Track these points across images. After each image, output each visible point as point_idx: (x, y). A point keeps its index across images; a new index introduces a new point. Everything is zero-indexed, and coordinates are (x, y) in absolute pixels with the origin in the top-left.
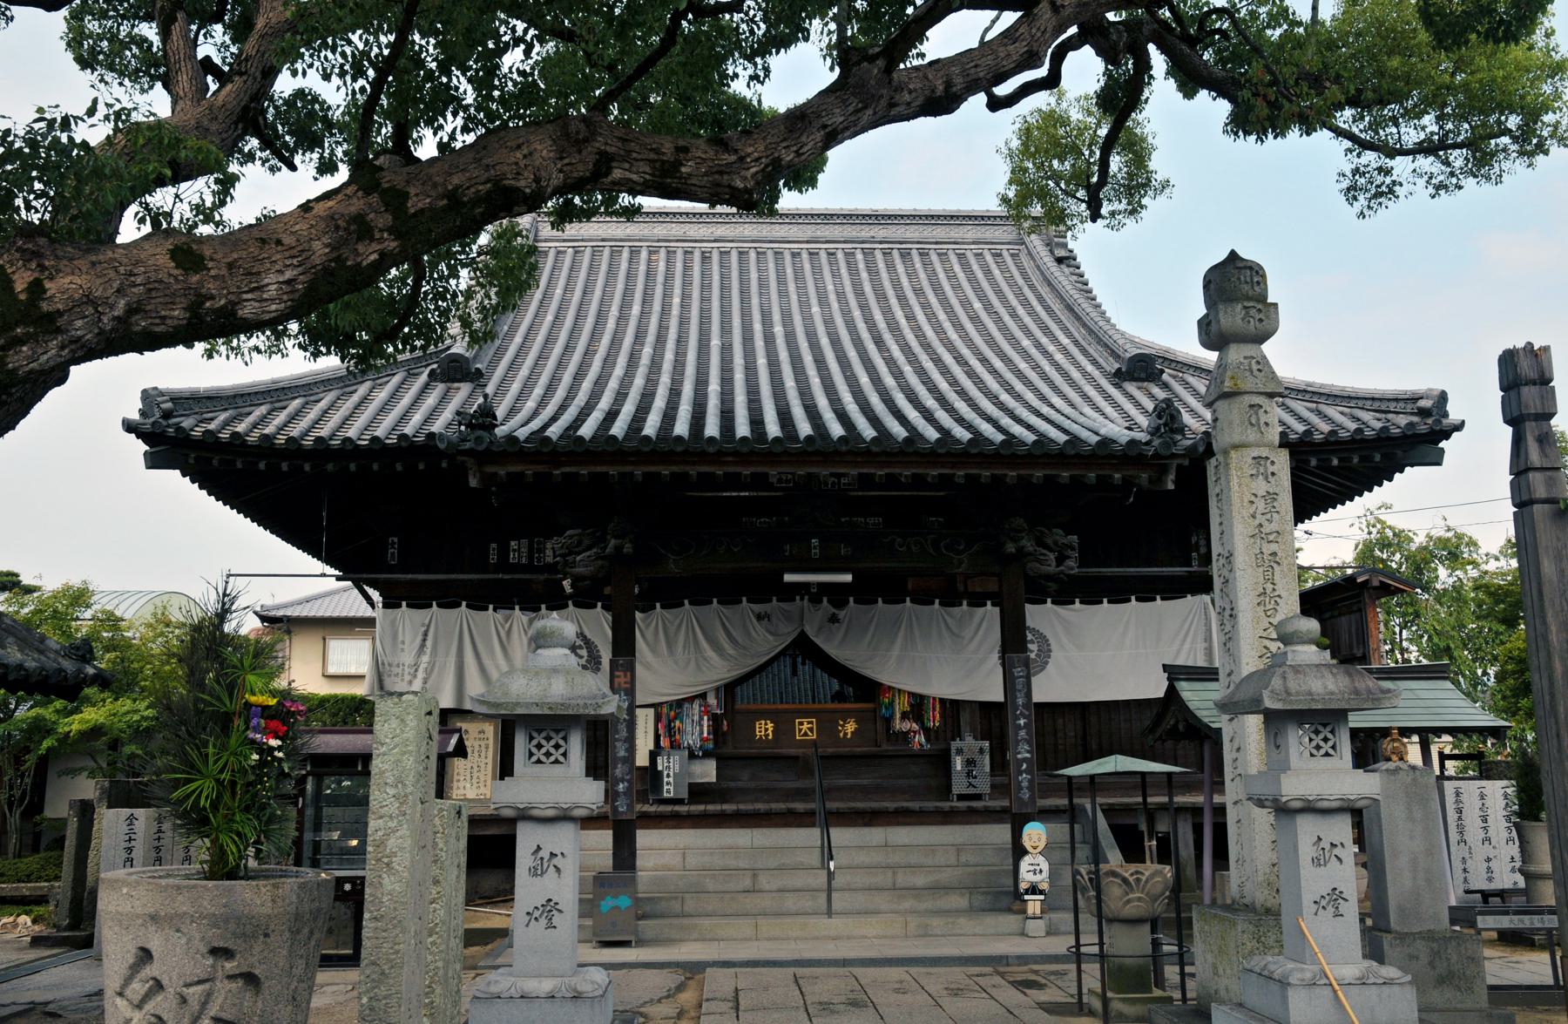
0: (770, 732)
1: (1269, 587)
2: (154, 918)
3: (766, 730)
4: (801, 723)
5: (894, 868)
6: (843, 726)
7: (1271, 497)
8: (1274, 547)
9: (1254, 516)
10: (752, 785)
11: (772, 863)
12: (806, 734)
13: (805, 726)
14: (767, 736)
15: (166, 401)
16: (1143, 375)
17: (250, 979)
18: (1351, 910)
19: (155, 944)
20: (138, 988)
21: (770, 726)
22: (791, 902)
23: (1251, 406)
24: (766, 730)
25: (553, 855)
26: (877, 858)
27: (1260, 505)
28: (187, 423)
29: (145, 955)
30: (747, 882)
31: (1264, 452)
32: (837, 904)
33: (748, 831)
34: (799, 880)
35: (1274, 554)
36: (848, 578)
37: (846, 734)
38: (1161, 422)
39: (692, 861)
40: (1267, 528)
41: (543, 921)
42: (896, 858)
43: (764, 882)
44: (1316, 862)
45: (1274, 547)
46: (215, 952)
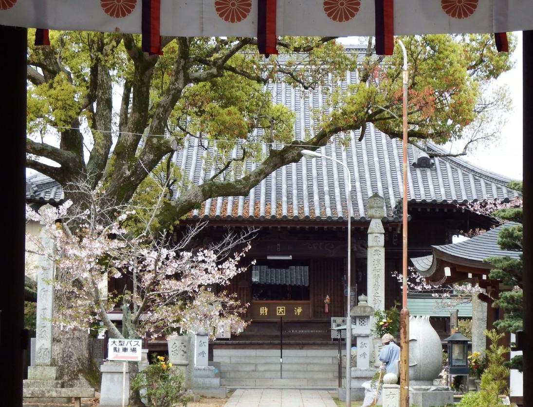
0: (266, 312)
1: (377, 283)
2: (176, 340)
3: (264, 311)
4: (279, 309)
5: (307, 364)
6: (296, 310)
7: (379, 260)
8: (379, 273)
9: (374, 265)
10: (258, 334)
11: (263, 361)
12: (281, 313)
13: (281, 310)
14: (265, 314)
15: (35, 187)
16: (425, 165)
17: (185, 346)
18: (367, 357)
19: (176, 342)
20: (174, 347)
21: (266, 309)
22: (268, 375)
23: (376, 236)
24: (264, 311)
25: (204, 343)
26: (301, 360)
27: (376, 262)
28: (42, 195)
29: (175, 343)
30: (253, 368)
31: (377, 248)
32: (284, 374)
33: (255, 350)
34: (272, 367)
35: (378, 275)
36: (290, 257)
37: (297, 313)
38: (396, 210)
39: (234, 360)
40: (378, 268)
41: (202, 355)
42: (308, 361)
43: (261, 368)
44: (361, 347)
45: (379, 273)
46: (182, 343)
